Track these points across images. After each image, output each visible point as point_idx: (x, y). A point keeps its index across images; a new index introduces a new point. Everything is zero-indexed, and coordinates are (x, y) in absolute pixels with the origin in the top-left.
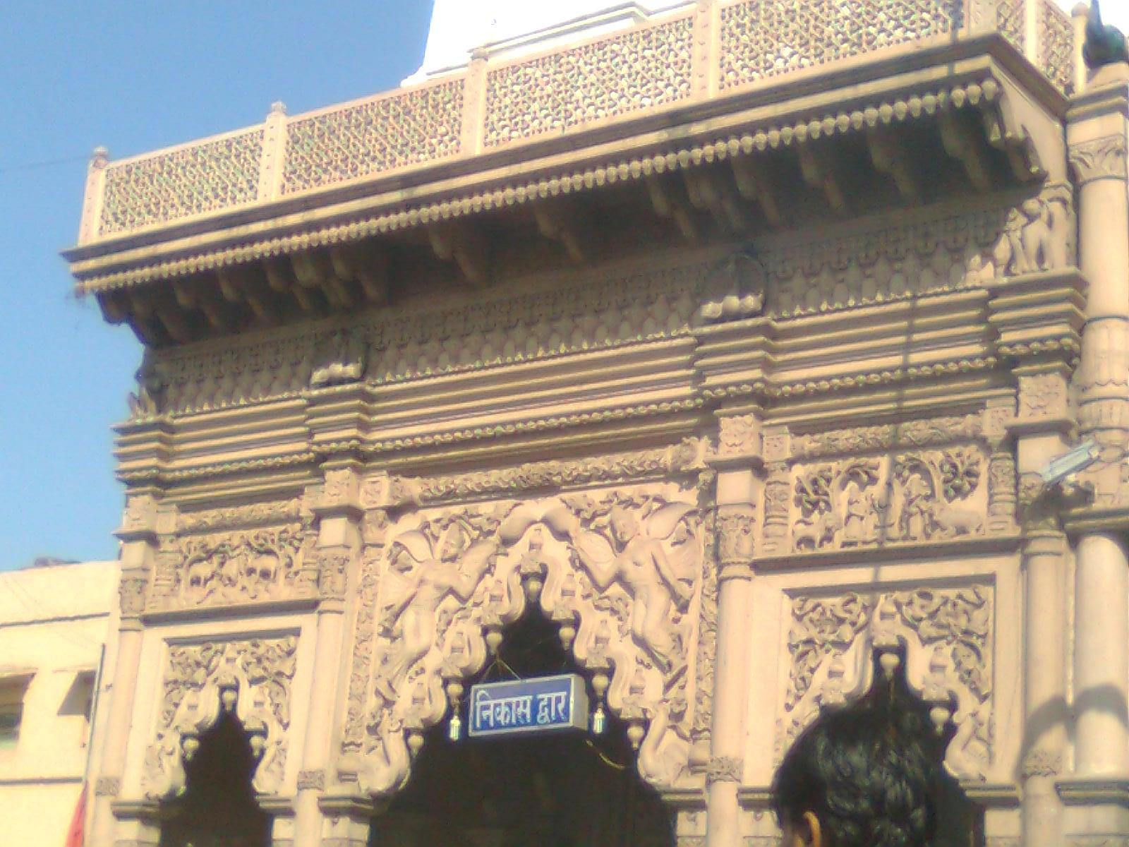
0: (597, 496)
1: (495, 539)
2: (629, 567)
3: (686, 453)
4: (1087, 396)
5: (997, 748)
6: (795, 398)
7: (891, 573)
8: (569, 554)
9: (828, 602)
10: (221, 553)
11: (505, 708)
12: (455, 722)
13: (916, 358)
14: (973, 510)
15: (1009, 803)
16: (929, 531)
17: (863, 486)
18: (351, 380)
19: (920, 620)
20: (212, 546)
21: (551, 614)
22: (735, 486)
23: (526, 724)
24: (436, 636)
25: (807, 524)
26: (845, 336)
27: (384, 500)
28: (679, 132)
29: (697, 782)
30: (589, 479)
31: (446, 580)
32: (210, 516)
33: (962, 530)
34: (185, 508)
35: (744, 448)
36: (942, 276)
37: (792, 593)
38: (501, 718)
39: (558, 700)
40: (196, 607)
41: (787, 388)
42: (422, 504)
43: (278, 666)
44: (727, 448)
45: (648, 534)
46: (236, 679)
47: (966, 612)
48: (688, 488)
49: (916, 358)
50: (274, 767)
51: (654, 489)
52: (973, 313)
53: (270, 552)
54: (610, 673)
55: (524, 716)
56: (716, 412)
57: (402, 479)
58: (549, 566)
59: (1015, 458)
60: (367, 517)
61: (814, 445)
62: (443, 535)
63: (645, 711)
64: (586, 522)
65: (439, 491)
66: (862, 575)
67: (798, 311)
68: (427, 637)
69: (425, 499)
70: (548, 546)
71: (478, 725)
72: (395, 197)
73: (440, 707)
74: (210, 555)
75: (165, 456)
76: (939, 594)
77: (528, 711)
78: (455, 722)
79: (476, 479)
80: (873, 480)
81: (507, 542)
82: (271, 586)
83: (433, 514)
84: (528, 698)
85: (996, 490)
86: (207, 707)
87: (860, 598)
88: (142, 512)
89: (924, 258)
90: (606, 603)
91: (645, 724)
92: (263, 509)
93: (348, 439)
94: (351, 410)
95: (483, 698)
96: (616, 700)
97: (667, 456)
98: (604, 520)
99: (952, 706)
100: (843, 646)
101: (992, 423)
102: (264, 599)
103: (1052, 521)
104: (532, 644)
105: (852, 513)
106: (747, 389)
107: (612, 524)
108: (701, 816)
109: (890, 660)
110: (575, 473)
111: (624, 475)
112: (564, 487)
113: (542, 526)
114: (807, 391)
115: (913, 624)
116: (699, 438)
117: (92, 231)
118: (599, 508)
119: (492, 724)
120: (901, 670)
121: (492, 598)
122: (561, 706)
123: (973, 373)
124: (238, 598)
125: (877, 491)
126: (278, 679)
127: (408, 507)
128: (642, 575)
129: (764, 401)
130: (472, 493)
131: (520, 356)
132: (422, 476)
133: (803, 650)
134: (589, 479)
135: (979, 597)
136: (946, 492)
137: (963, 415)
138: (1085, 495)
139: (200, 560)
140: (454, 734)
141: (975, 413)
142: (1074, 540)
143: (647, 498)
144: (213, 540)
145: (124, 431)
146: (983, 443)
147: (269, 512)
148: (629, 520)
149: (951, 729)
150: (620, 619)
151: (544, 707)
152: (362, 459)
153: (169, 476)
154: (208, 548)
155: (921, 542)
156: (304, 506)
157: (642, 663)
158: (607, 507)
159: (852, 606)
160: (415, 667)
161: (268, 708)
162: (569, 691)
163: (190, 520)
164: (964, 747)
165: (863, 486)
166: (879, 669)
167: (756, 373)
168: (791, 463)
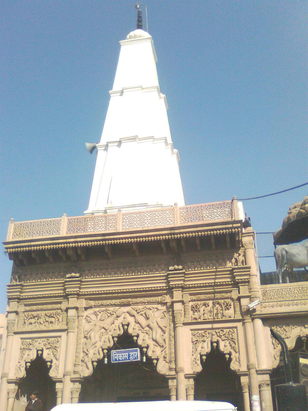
0: (141, 307)
1: (115, 316)
2: (151, 323)
3: (164, 298)
4: (252, 290)
5: (242, 363)
6: (189, 288)
7: (215, 326)
8: (134, 320)
9: (200, 332)
10: (38, 317)
11: (120, 356)
12: (106, 359)
13: (217, 281)
14: (230, 313)
15: (61, 382)
16: (222, 317)
17: (206, 307)
18: (77, 277)
19: (221, 336)
20: (35, 315)
21: (131, 334)
22: (178, 307)
23: (127, 360)
24: (99, 339)
25: (194, 315)
26: (201, 276)
27: (84, 306)
28: (173, 231)
29: (173, 373)
30: (138, 303)
31: (102, 325)
32: (34, 308)
33: (230, 317)
34: (26, 305)
35: (14, 308)
36: (220, 265)
37: (22, 339)
38: (120, 359)
39: (135, 354)
40: (31, 330)
41: (188, 286)
42: (93, 307)
43: (55, 345)
44: (176, 298)
45: (154, 316)
46: (42, 348)
47: (231, 334)
48: (163, 306)
49: (217, 281)
50: (55, 370)
51: (155, 306)
52: (62, 285)
53: (52, 317)
54: (147, 347)
55: (126, 358)
56: (173, 290)
57: (89, 301)
58: (130, 323)
59: (67, 313)
60: (79, 309)
61: (195, 298)
62: (100, 315)
63: (157, 357)
64: (138, 313)
65: (99, 304)
66: (209, 326)
67: (190, 270)
68: (97, 339)
69: (95, 306)
70: (122, 317)
71: (114, 360)
72: (100, 238)
73: (102, 355)
74: (34, 317)
75: (21, 292)
76: (225, 330)
77: (127, 357)
78: (106, 359)
79: (109, 302)
80: (208, 306)
81: (118, 317)
82: (53, 325)
83: (97, 309)
84: (127, 354)
85: (236, 309)
86: (33, 356)
87: (207, 331)
88: (14, 305)
89: (217, 261)
90: (145, 332)
91: (157, 359)
92: (50, 306)
93: (76, 291)
94: (19, 288)
95: (115, 354)
96: (150, 354)
97: (159, 299)
98: (143, 313)
99: (51, 362)
100: (204, 341)
101: (235, 295)
102: (51, 328)
103: (249, 316)
104: (126, 340)
105: (205, 312)
106: (180, 285)
107: (145, 313)
108: (175, 381)
109: (40, 352)
110: (136, 302)
111: (148, 303)
112: (132, 305)
113: (127, 313)
114: (99, 293)
115: (220, 337)
116: (167, 295)
117: (10, 238)
118: (141, 310)
119: (118, 360)
120: (218, 346)
121: (114, 330)
122: (136, 356)
123: (61, 296)
124: (43, 328)
125: (209, 308)
126: (55, 348)
127: (91, 307)
128: (154, 325)
129: (183, 288)
130: (108, 305)
131: (103, 276)
132: (94, 300)
133: (195, 343)
134: (138, 303)
135: (234, 331)
136: (225, 309)
137: (227, 293)
138: (254, 310)
139: (31, 318)
140: (106, 362)
141: (60, 304)
142: (253, 320)
143: (154, 308)
144: (35, 314)
145: (9, 286)
146: (232, 299)
147: (52, 307)
148: (149, 313)
149: (51, 366)
150: (149, 335)
151: (131, 356)
152: (79, 295)
153: (21, 297)
154: (34, 315)
155: (221, 319)
156: (64, 306)
157: (155, 345)
158: (144, 310)
159: (206, 333)
160: (94, 346)
161: (52, 355)
162: (138, 352)
163: (28, 308)
164: (234, 363)
165: (206, 307)
166: (37, 354)
167: (182, 282)
168: (190, 301)
